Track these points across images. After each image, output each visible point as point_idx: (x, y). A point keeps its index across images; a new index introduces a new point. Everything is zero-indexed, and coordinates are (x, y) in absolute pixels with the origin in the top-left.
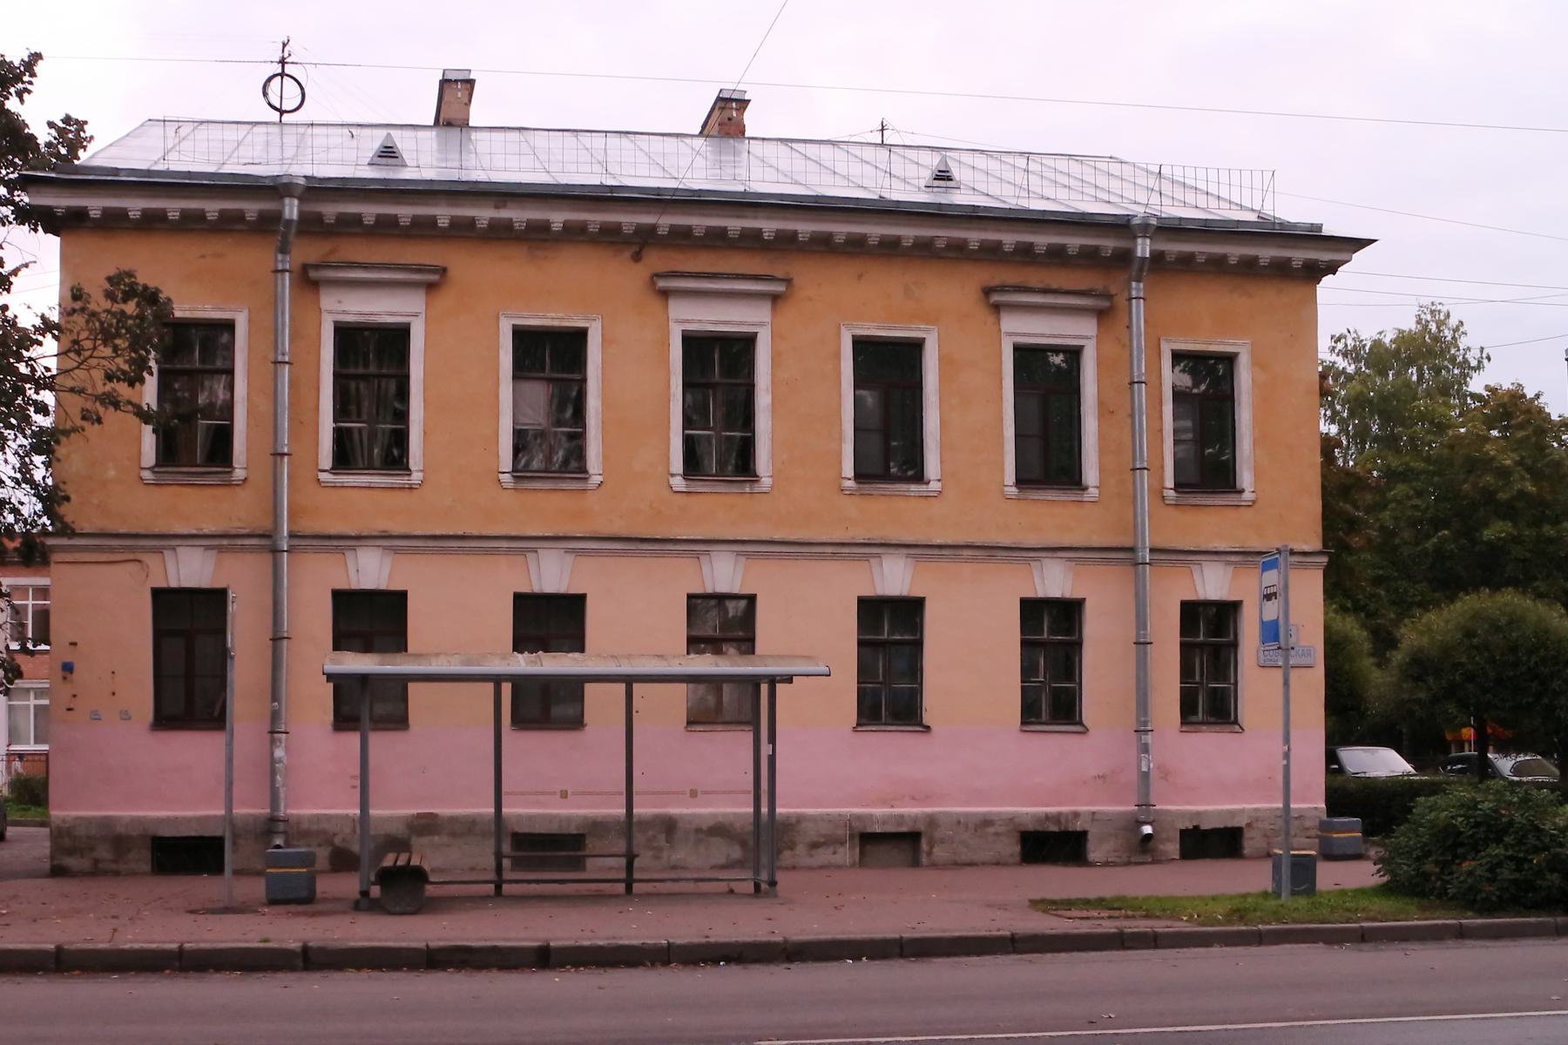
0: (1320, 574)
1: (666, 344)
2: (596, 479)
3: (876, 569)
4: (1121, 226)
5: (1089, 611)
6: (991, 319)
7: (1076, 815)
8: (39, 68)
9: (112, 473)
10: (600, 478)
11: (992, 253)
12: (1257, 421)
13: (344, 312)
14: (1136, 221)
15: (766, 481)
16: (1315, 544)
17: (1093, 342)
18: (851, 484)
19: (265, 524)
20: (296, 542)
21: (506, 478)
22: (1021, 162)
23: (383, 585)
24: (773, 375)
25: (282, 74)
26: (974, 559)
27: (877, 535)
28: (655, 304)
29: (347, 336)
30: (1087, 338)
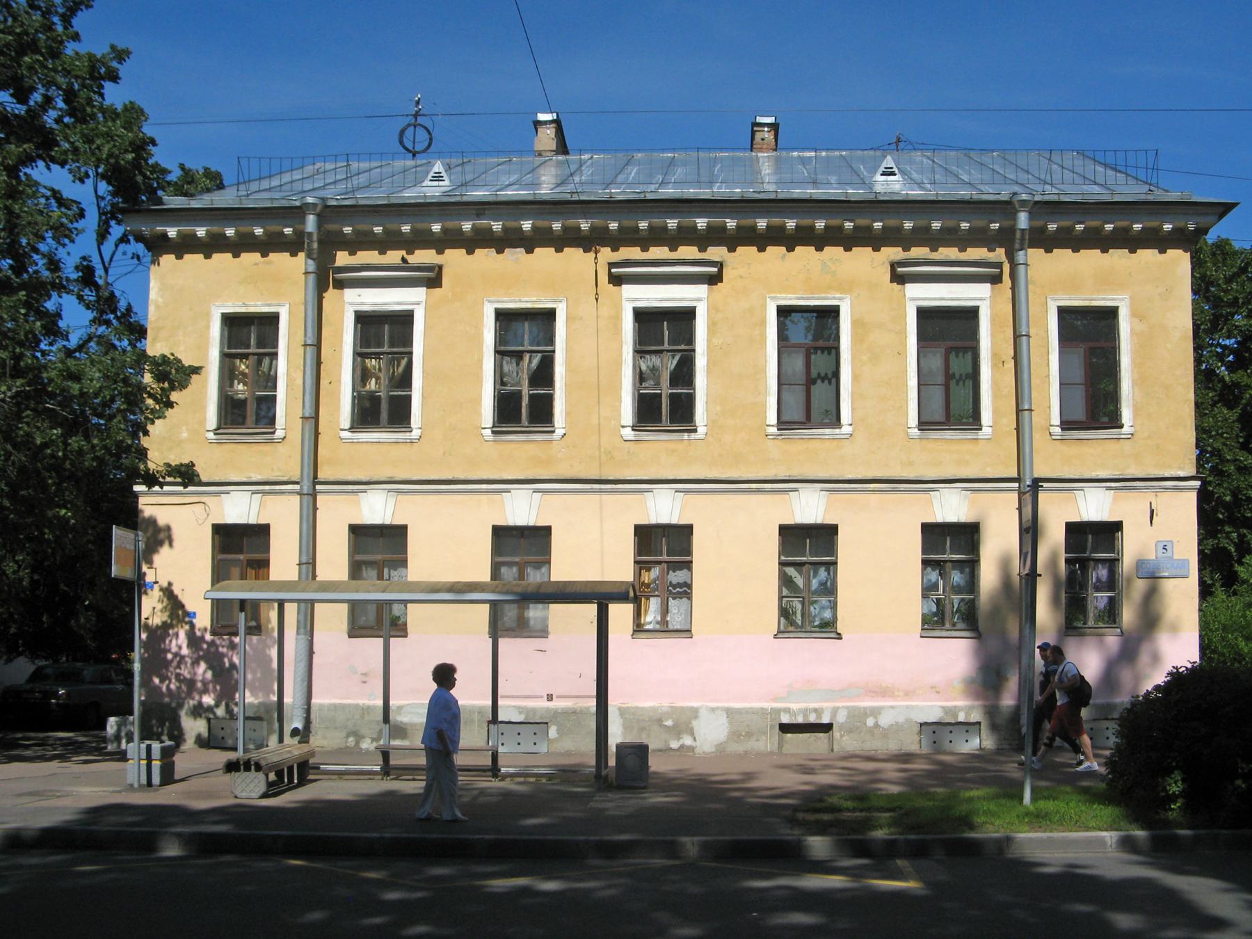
0: (1192, 497)
1: (617, 318)
8: (187, 166)
9: (185, 435)
10: (563, 431)
12: (1135, 364)
13: (362, 304)
15: (701, 430)
16: (1191, 470)
17: (987, 303)
23: (675, 520)
24: (708, 341)
27: (796, 473)
29: (366, 321)
30: (981, 299)
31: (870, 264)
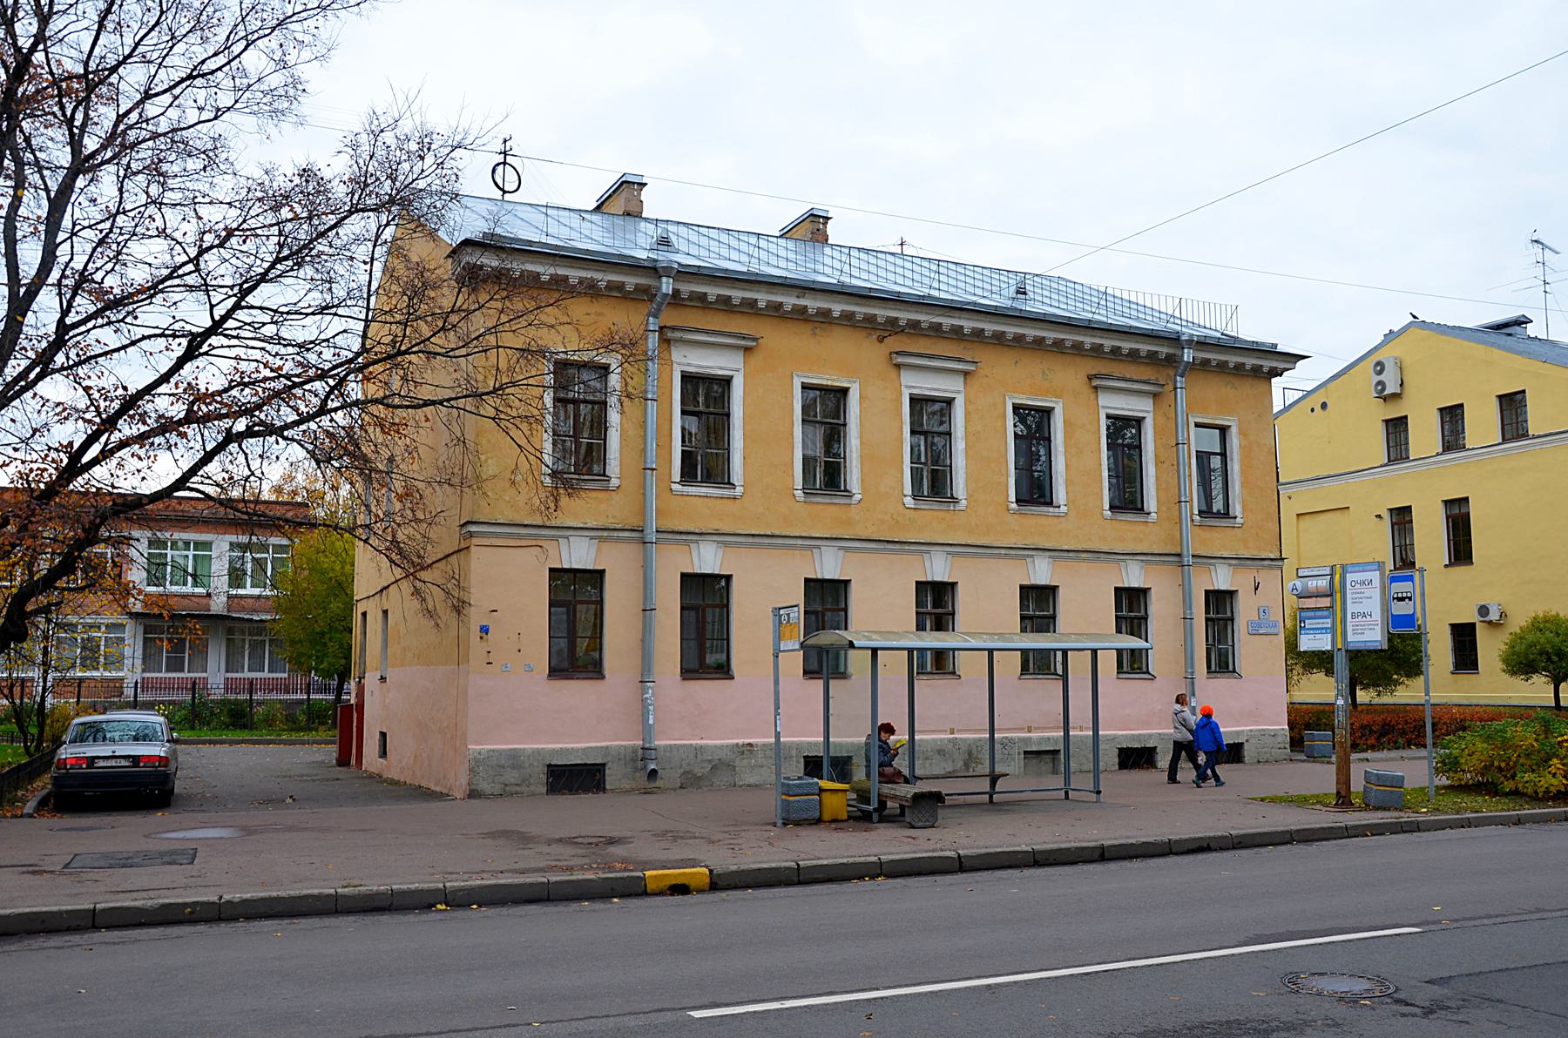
2: (858, 497)
3: (1030, 567)
4: (1174, 340)
5: (1154, 597)
6: (1093, 396)
7: (1150, 736)
11: (1097, 351)
14: (1184, 338)
18: (1014, 506)
19: (634, 522)
20: (660, 536)
21: (799, 493)
22: (753, 240)
25: (505, 163)
26: (1088, 559)
27: (1030, 542)
28: (892, 372)
31: (1070, 375)
